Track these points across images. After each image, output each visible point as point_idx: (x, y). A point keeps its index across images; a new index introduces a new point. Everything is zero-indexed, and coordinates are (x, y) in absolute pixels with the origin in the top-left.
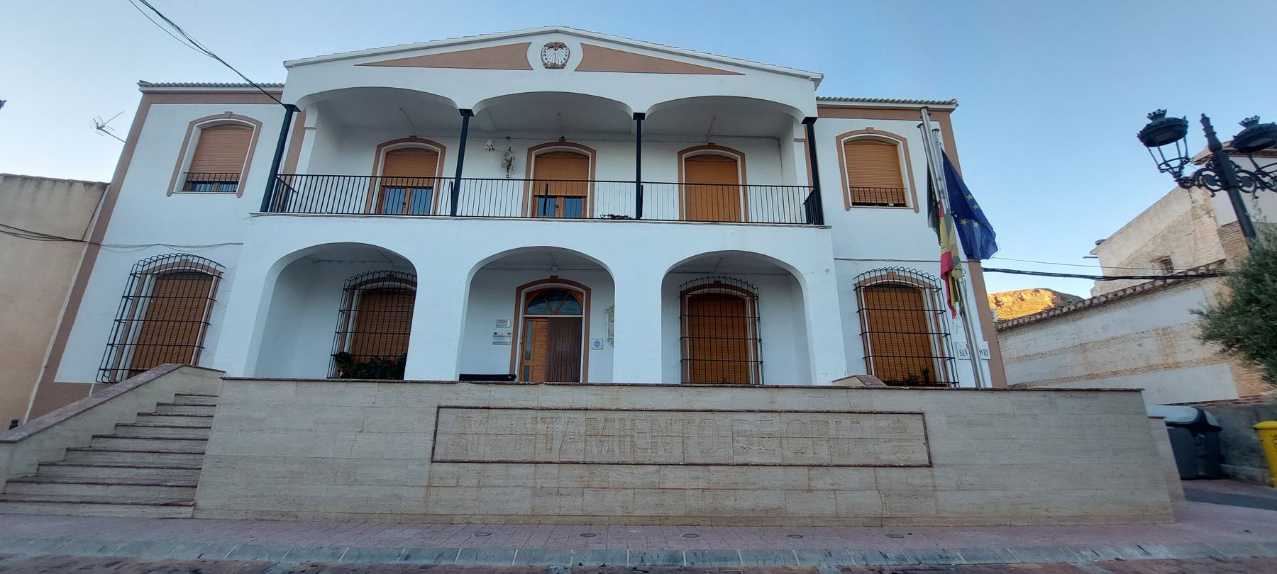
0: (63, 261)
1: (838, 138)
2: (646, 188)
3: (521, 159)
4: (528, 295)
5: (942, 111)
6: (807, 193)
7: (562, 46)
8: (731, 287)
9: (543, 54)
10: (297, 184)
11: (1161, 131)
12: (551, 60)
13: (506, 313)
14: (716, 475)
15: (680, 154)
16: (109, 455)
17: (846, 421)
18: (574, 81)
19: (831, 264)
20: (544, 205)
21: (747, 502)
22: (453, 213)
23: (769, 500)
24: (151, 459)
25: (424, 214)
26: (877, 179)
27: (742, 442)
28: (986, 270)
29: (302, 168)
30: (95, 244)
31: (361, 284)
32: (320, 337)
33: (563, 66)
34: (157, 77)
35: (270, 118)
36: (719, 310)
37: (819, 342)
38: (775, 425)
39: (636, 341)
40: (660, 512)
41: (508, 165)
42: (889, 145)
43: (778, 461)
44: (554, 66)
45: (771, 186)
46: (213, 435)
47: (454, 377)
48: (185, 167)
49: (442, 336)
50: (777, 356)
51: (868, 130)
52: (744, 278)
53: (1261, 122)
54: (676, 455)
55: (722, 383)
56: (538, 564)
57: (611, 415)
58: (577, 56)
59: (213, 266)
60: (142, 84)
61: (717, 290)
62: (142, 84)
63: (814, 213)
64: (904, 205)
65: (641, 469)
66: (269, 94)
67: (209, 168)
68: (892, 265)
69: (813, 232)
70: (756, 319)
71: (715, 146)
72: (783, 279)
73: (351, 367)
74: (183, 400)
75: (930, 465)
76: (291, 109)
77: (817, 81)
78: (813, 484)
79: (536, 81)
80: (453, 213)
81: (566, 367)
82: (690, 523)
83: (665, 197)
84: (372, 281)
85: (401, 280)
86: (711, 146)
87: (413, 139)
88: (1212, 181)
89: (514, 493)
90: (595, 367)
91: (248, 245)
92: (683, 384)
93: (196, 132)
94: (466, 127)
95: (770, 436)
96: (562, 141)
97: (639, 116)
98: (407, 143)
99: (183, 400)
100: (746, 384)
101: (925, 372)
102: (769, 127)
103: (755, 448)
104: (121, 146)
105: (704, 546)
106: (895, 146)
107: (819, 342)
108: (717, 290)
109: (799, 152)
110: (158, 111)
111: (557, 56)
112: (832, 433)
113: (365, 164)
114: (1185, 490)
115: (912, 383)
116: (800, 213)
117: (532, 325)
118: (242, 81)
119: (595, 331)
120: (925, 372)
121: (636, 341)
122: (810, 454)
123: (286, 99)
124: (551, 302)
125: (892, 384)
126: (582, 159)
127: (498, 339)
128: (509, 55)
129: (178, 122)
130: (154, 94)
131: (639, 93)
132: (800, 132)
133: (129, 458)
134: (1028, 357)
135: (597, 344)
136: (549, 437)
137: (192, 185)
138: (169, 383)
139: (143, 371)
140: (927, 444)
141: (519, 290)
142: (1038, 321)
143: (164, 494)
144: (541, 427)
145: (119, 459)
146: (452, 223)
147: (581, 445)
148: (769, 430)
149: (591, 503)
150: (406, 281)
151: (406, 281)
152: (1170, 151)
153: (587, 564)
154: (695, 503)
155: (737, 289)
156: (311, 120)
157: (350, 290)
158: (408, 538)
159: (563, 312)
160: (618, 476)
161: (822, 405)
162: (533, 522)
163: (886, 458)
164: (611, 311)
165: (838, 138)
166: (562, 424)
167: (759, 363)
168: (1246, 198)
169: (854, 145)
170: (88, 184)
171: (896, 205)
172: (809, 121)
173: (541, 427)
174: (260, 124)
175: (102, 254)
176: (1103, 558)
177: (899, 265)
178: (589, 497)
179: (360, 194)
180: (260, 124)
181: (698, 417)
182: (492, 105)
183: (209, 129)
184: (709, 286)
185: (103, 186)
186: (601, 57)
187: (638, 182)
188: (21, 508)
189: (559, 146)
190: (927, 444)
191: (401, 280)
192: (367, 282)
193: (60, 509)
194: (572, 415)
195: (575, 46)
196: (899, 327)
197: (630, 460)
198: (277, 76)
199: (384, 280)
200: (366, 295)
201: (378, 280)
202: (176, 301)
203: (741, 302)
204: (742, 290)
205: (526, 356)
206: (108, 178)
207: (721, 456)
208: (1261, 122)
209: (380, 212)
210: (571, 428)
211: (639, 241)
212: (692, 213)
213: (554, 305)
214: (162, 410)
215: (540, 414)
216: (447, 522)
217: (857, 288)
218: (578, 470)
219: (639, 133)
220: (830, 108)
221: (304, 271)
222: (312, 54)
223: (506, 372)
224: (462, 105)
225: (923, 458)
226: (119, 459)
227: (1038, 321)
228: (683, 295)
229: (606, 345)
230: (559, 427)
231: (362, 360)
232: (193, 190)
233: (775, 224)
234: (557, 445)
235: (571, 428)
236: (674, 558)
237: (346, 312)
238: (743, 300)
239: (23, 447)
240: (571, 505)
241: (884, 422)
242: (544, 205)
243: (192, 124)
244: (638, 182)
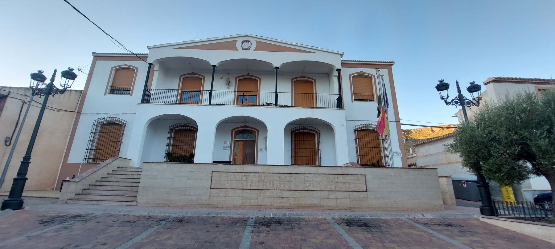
0: (69, 118)
1: (350, 75)
2: (279, 95)
3: (233, 81)
4: (235, 132)
5: (388, 66)
6: (337, 96)
7: (249, 41)
8: (310, 130)
9: (242, 44)
10: (152, 92)
11: (442, 86)
12: (245, 47)
13: (228, 140)
14: (299, 194)
15: (292, 80)
16: (103, 187)
17: (341, 177)
18: (253, 55)
19: (345, 123)
20: (243, 99)
21: (309, 202)
22: (210, 104)
23: (316, 201)
24: (117, 188)
25: (197, 104)
26: (364, 91)
27: (307, 183)
28: (403, 124)
29: (153, 86)
30: (79, 113)
31: (175, 128)
32: (161, 147)
33: (249, 49)
34: (98, 51)
35: (142, 68)
36: (305, 139)
37: (340, 150)
38: (318, 178)
39: (275, 149)
40: (281, 205)
41: (228, 84)
42: (369, 78)
43: (319, 189)
44: (246, 49)
45: (325, 93)
46: (141, 181)
47: (211, 162)
48: (110, 85)
49: (206, 147)
50: (326, 155)
51: (361, 72)
52: (313, 126)
53: (475, 84)
54: (287, 187)
55: (301, 165)
56: (246, 216)
57: (267, 174)
58: (254, 45)
59: (123, 121)
60: (93, 53)
61: (305, 131)
62: (93, 53)
63: (340, 104)
64: (373, 100)
65: (276, 191)
66: (142, 58)
67: (119, 85)
68: (368, 123)
69: (339, 111)
70: (319, 142)
71: (305, 78)
72: (328, 127)
73: (173, 158)
74: (120, 169)
75: (366, 191)
76: (150, 64)
77: (342, 55)
78: (330, 197)
79: (239, 54)
80: (210, 104)
81: (249, 157)
82: (291, 207)
83: (286, 98)
84: (179, 126)
85: (190, 126)
86: (304, 77)
87: (193, 73)
88: (457, 103)
89: (236, 198)
90: (260, 158)
91: (137, 116)
92: (292, 165)
93: (114, 71)
94: (214, 71)
95: (316, 182)
96: (248, 75)
97: (277, 68)
98: (190, 76)
99: (120, 169)
100: (315, 165)
101: (378, 161)
102: (325, 72)
103: (312, 185)
104: (87, 76)
105: (294, 212)
106: (371, 78)
107: (340, 150)
108: (305, 131)
109: (335, 80)
110: (99, 63)
111: (247, 45)
112: (336, 181)
113: (175, 84)
114: (456, 202)
115: (373, 165)
116: (334, 103)
117: (237, 143)
118: (128, 53)
119: (260, 145)
120: (378, 161)
121: (275, 149)
122: (329, 187)
123: (150, 60)
124: (244, 135)
125: (363, 166)
126: (255, 81)
127: (225, 148)
128: (228, 44)
129: (106, 69)
130: (98, 57)
131: (277, 59)
132: (336, 73)
133: (110, 188)
134: (427, 155)
135: (261, 150)
136: (247, 181)
137: (112, 91)
138: (112, 165)
139: (107, 159)
140: (366, 185)
141: (232, 130)
142: (430, 142)
143: (125, 199)
144: (244, 178)
145: (107, 188)
146: (210, 107)
147: (257, 184)
148: (316, 180)
149: (260, 202)
150: (194, 128)
151: (194, 128)
152: (444, 93)
153: (260, 216)
154: (292, 202)
155: (312, 130)
156: (156, 67)
157: (171, 130)
158: (207, 210)
159: (248, 138)
160: (268, 193)
161: (337, 172)
162: (242, 207)
163: (353, 189)
164: (266, 138)
165: (350, 75)
166: (251, 177)
167: (319, 158)
168: (467, 108)
169: (355, 78)
170: (76, 91)
171: (370, 100)
172: (339, 70)
173: (244, 178)
174: (137, 69)
175: (82, 116)
176: (411, 217)
177: (370, 123)
178: (260, 200)
179: (174, 96)
180: (137, 69)
181: (294, 175)
182: (223, 64)
183: (118, 70)
184: (302, 129)
185: (81, 91)
186: (263, 46)
187: (276, 92)
188: (83, 202)
189: (247, 78)
190: (366, 185)
191: (190, 126)
192: (177, 127)
193: (91, 202)
194: (253, 174)
195: (253, 41)
196: (370, 146)
197: (272, 189)
198: (144, 51)
199: (183, 126)
200: (176, 131)
201: (182, 126)
202: (110, 134)
203: (313, 135)
204: (314, 131)
205: (235, 154)
206: (82, 89)
207: (301, 187)
208: (475, 84)
209: (181, 103)
210: (254, 179)
211: (276, 117)
212: (296, 104)
213: (245, 135)
214: (114, 173)
215: (244, 174)
216: (216, 207)
217: (355, 131)
218: (256, 192)
219: (277, 73)
220: (346, 64)
221: (156, 124)
222: (158, 44)
223: (228, 160)
224: (212, 64)
225: (365, 189)
226: (107, 188)
227: (430, 142)
228: (292, 132)
229: (264, 151)
230: (250, 178)
231: (176, 155)
232: (113, 93)
233: (325, 108)
234: (249, 184)
235: (254, 179)
236: (285, 215)
237: (170, 138)
238: (314, 134)
239: (79, 184)
240: (254, 202)
241: (353, 177)
242: (243, 99)
243: (112, 68)
244: (276, 92)
